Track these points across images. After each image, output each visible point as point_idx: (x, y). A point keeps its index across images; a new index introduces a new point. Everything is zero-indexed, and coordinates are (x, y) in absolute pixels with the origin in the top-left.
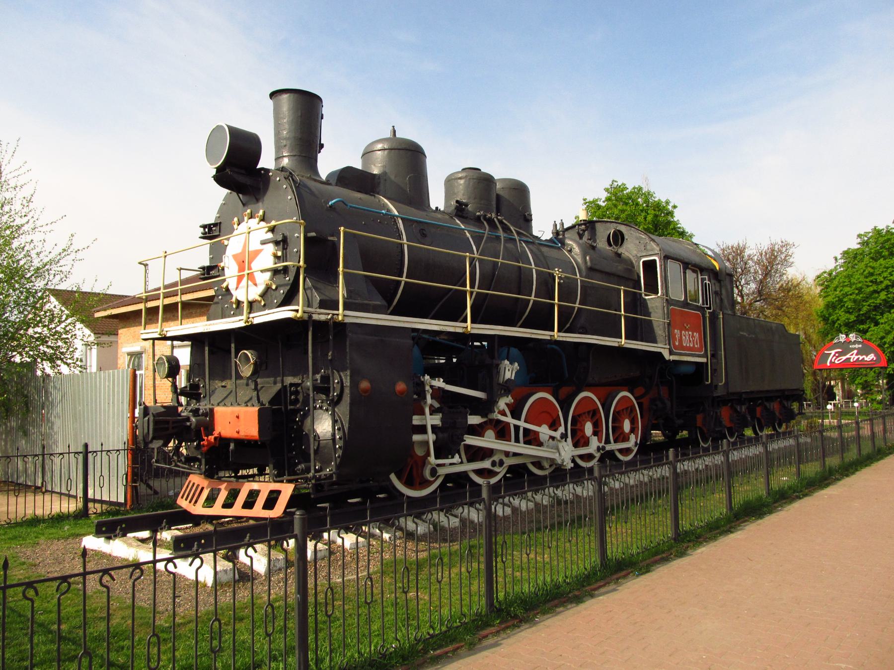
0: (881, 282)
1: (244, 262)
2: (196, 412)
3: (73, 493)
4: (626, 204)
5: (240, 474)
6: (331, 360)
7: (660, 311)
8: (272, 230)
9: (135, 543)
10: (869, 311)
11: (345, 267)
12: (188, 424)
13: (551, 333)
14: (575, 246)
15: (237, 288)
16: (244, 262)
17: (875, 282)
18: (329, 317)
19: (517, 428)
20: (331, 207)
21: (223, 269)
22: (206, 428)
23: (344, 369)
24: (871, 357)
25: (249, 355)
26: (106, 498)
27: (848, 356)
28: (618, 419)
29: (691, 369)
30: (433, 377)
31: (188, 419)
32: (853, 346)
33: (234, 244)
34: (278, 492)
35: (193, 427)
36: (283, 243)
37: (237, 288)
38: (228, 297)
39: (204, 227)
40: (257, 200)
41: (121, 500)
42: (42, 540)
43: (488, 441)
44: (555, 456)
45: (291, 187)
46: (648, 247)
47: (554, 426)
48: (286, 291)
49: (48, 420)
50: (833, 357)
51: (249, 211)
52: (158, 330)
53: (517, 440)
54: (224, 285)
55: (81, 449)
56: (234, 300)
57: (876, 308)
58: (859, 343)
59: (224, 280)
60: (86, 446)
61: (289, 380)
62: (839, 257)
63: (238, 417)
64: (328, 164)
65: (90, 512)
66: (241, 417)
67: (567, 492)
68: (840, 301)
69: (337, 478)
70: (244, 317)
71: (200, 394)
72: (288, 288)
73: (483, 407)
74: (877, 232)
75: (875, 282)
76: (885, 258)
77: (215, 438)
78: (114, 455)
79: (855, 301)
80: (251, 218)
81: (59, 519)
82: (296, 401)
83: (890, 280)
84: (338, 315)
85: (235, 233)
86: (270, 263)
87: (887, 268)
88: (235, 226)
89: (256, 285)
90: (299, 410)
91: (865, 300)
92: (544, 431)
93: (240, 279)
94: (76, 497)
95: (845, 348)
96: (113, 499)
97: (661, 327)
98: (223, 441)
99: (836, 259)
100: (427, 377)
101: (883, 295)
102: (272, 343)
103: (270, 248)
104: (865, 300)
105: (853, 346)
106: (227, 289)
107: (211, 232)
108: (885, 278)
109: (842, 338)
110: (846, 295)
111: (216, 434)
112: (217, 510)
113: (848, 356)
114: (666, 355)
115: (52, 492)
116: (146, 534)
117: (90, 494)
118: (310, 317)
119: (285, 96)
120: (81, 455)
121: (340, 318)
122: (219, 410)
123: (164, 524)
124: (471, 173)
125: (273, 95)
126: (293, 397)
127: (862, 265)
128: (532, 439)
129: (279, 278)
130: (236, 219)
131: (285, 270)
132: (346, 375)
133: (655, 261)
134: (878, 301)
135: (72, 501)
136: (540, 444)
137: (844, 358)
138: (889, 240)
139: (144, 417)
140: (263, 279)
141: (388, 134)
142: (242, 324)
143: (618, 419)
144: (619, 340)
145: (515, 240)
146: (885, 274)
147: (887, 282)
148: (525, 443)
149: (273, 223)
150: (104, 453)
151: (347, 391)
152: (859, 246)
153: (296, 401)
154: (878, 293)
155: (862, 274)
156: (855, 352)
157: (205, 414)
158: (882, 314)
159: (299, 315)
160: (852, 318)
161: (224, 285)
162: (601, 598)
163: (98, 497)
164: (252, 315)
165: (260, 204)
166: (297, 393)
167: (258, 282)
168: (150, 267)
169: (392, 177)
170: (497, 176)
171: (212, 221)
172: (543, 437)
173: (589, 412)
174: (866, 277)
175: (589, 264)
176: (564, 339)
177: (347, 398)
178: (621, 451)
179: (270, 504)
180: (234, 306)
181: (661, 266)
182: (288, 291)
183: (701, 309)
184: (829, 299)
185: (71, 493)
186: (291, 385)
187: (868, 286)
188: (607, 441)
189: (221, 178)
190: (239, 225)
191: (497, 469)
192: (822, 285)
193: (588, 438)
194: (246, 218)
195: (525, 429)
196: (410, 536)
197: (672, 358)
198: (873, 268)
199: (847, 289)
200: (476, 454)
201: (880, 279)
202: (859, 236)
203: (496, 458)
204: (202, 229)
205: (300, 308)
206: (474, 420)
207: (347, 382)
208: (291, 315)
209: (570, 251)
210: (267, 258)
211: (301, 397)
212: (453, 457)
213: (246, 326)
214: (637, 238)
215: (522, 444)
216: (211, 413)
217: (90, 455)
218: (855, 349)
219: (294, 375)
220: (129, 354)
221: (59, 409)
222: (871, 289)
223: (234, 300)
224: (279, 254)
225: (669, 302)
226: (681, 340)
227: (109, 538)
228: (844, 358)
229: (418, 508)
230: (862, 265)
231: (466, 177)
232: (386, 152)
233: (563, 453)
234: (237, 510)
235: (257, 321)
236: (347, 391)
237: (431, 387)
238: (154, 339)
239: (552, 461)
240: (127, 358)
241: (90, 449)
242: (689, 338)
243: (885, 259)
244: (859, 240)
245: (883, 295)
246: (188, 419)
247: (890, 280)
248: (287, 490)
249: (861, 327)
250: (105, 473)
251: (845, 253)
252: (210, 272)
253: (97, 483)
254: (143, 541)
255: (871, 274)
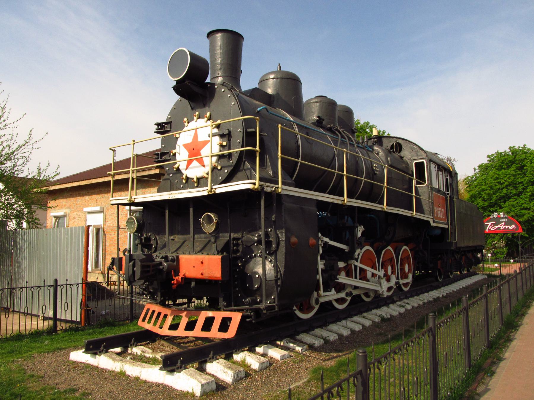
0: (503, 183)
1: (194, 151)
2: (166, 258)
3: (35, 312)
4: (361, 132)
5: (177, 302)
6: (274, 222)
7: (427, 195)
8: (218, 126)
9: (114, 356)
10: (496, 200)
11: (282, 153)
12: (161, 267)
13: (382, 206)
14: (380, 151)
15: (187, 169)
16: (194, 151)
17: (501, 184)
18: (274, 189)
19: (356, 267)
20: (258, 112)
21: (174, 155)
22: (175, 271)
23: (280, 228)
24: (513, 227)
25: (213, 216)
26: (69, 318)
27: (499, 226)
28: (402, 265)
29: (438, 232)
30: (324, 235)
31: (161, 264)
32: (502, 220)
33: (184, 138)
34: (230, 319)
35: (165, 270)
36: (226, 136)
37: (187, 169)
38: (178, 175)
39: (158, 124)
40: (204, 105)
41: (79, 320)
42: (34, 353)
43: (342, 279)
44: (378, 288)
45: (234, 96)
46: (419, 154)
47: (373, 267)
48: (230, 170)
49: (16, 262)
50: (489, 226)
51: (197, 113)
52: (128, 198)
53: (356, 278)
54: (176, 166)
55: (52, 283)
56: (184, 177)
57: (501, 198)
58: (506, 218)
59: (176, 163)
60: (56, 281)
61: (233, 235)
62: (477, 168)
63: (202, 263)
64: (248, 82)
65: (58, 329)
66: (205, 263)
67: (386, 311)
68: (479, 194)
69: (279, 308)
70: (208, 188)
71: (152, 245)
72: (231, 168)
73: (347, 256)
74: (499, 154)
75: (501, 184)
76: (505, 169)
77: (182, 278)
78: (75, 287)
79: (488, 194)
80: (199, 118)
81: (37, 335)
82: (237, 251)
83: (508, 182)
84: (278, 188)
85: (184, 130)
86: (216, 150)
87: (507, 175)
88: (186, 124)
89: (204, 166)
90: (240, 258)
91: (494, 193)
92: (370, 271)
93: (189, 162)
94: (38, 316)
95: (497, 221)
96: (74, 319)
97: (428, 205)
98: (187, 280)
99: (475, 169)
100: (320, 235)
101: (505, 191)
102: (232, 209)
103: (217, 140)
104: (494, 193)
105: (502, 220)
106: (178, 169)
107: (162, 128)
108: (505, 181)
109: (496, 215)
110: (483, 190)
111: (181, 275)
112: (181, 332)
113: (499, 226)
114: (432, 224)
115: (20, 312)
116: (119, 350)
117: (58, 317)
118: (263, 188)
119: (219, 36)
120: (52, 287)
121: (280, 190)
122: (181, 256)
123: (133, 342)
124: (319, 99)
125: (210, 34)
126: (235, 248)
127: (491, 173)
128: (363, 275)
129: (225, 161)
130: (185, 119)
131: (230, 156)
132: (282, 233)
133: (423, 162)
134: (502, 194)
135: (35, 319)
136: (368, 281)
137: (497, 227)
138: (506, 159)
139: (130, 262)
140: (209, 162)
141: (276, 69)
142: (205, 193)
143: (402, 265)
144: (412, 212)
145: (354, 145)
146: (506, 179)
147: (506, 183)
148: (360, 279)
149: (219, 122)
150: (68, 286)
151: (282, 244)
152: (488, 162)
153: (237, 251)
154: (502, 189)
155: (492, 178)
156: (504, 223)
157: (173, 260)
158: (505, 202)
159: (256, 186)
160: (486, 204)
161: (176, 166)
162: (486, 396)
163: (63, 318)
164: (214, 187)
165: (207, 108)
166: (237, 245)
167: (205, 164)
168: (116, 152)
169: (283, 97)
170: (339, 103)
171: (163, 120)
172: (369, 275)
173: (389, 259)
174: (494, 180)
175: (390, 162)
176: (399, 209)
177: (282, 250)
178: (404, 284)
179: (224, 327)
180: (184, 181)
181: (427, 166)
182: (231, 170)
183: (444, 194)
184: (472, 192)
185: (21, 311)
186: (234, 239)
187: (496, 185)
188: (398, 278)
189: (179, 88)
190: (188, 123)
191: (347, 298)
192: (467, 184)
193: (390, 276)
194: (195, 118)
195: (360, 268)
196: (311, 347)
197: (434, 225)
198: (498, 175)
199: (484, 187)
200: (340, 288)
201: (503, 181)
202: (488, 156)
203: (347, 290)
204: (156, 126)
205: (257, 182)
206: (341, 264)
207: (282, 237)
208: (250, 186)
209: (378, 154)
210: (213, 147)
211: (240, 248)
212: (330, 291)
213: (209, 195)
214: (411, 148)
215: (358, 280)
216: (177, 260)
217: (58, 287)
218: (503, 222)
219: (235, 232)
220: (55, 217)
221: (26, 254)
222: (498, 187)
223: (184, 177)
224: (225, 143)
225: (432, 189)
226: (437, 215)
227: (96, 354)
228: (497, 227)
229: (309, 327)
230: (491, 173)
231: (320, 101)
232: (279, 80)
233: (383, 287)
234: (197, 332)
235: (218, 191)
236: (282, 244)
237: (322, 241)
238: (118, 205)
239: (376, 291)
240: (53, 220)
241: (58, 284)
242: (440, 212)
243: (505, 170)
244: (488, 159)
245: (505, 191)
246: (161, 264)
247: (508, 182)
248: (236, 317)
249: (492, 209)
250: (69, 301)
251: (480, 167)
252: (162, 156)
253: (63, 308)
254: (119, 354)
255: (497, 178)
